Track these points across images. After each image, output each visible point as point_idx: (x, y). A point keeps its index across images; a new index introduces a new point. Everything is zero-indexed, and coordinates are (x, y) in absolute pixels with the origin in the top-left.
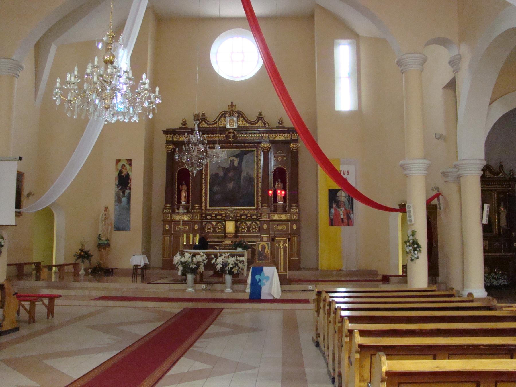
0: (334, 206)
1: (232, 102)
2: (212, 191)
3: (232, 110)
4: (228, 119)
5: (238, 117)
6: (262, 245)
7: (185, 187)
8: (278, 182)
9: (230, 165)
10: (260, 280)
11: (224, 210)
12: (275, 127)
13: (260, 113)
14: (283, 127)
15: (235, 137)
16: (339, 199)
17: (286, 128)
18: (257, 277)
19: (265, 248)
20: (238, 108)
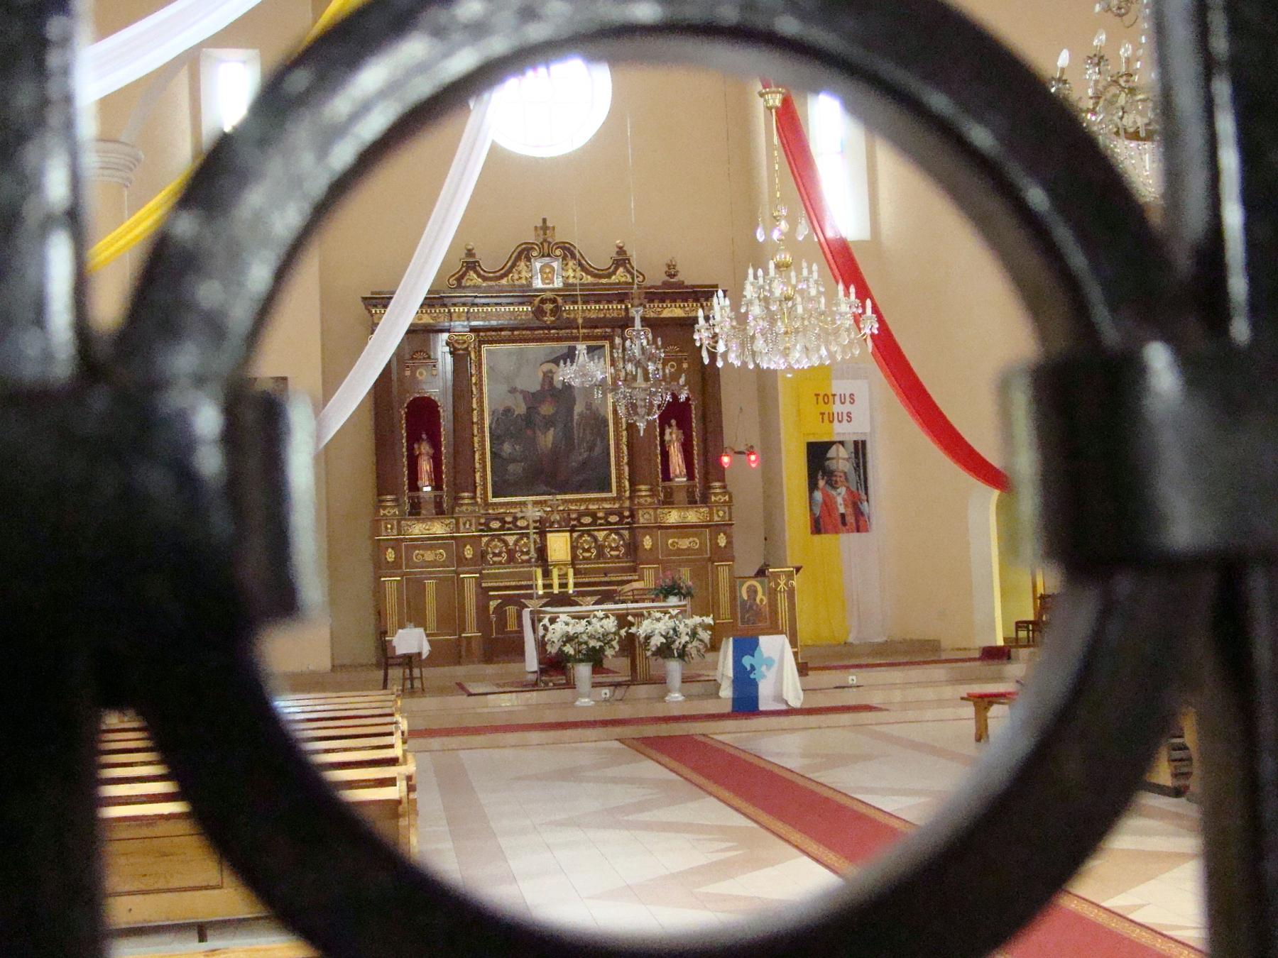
0: (821, 483)
1: (544, 221)
2: (500, 457)
3: (545, 240)
4: (538, 265)
5: (564, 258)
6: (749, 587)
7: (425, 448)
8: (670, 426)
9: (542, 386)
10: (753, 668)
11: (582, 501)
12: (659, 283)
13: (621, 248)
14: (681, 285)
15: (556, 311)
16: (832, 465)
17: (687, 287)
18: (747, 661)
19: (756, 592)
20: (559, 237)
